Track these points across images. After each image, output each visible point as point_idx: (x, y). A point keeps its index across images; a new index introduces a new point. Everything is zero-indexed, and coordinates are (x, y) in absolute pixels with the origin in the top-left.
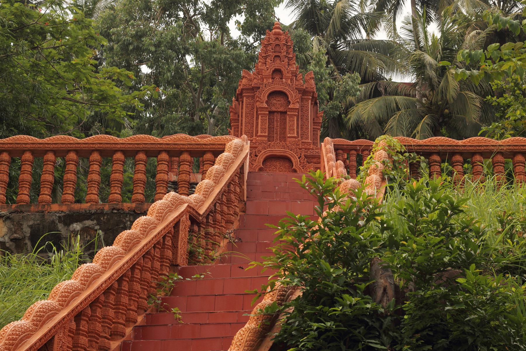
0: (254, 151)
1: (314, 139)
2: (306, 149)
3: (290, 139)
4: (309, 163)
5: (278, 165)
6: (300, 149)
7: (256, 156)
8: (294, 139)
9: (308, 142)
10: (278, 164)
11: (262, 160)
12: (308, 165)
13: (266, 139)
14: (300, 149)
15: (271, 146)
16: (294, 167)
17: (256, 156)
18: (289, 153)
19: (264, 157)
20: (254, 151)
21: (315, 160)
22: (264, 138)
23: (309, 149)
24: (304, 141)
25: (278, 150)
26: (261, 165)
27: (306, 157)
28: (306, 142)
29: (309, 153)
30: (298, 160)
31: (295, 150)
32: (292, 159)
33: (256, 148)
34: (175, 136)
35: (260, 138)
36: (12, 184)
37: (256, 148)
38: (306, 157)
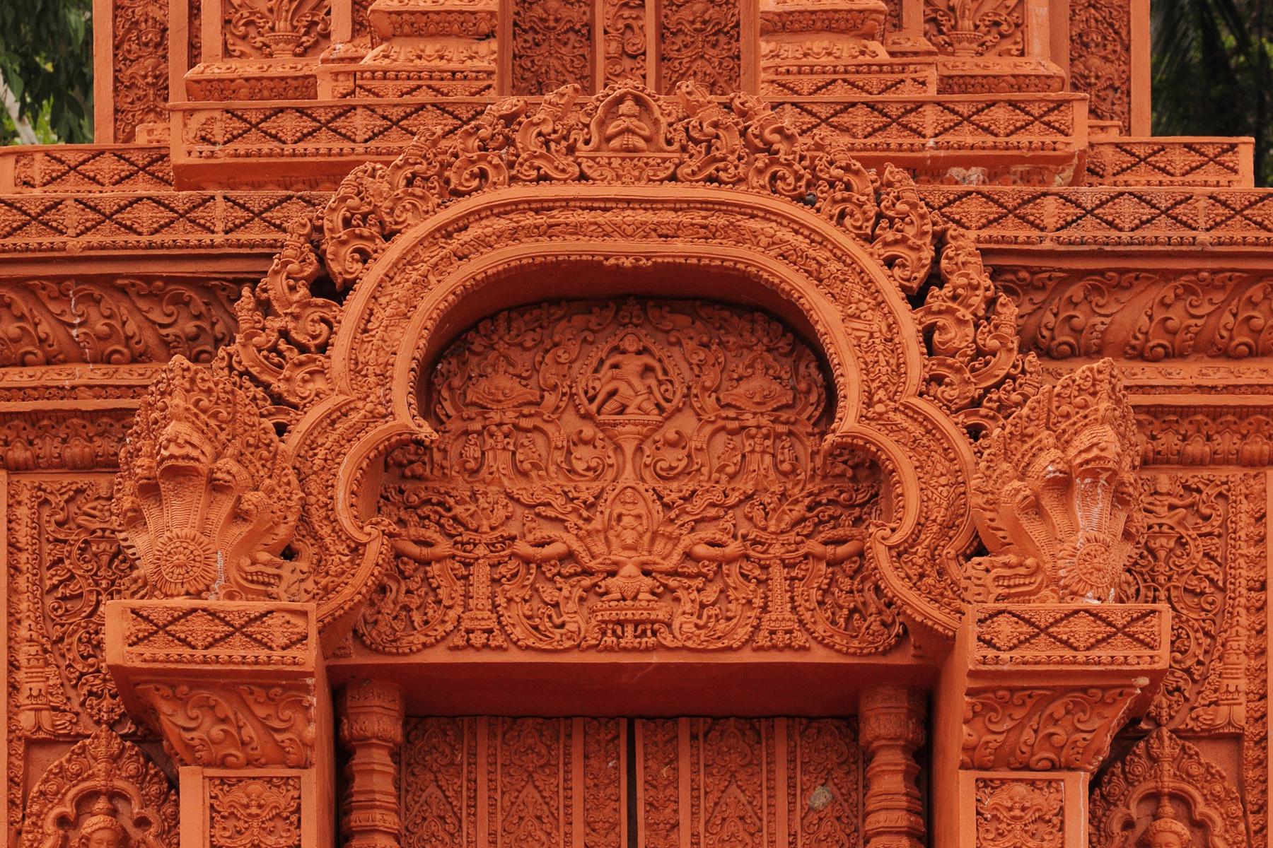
0: (297, 216)
1: (1080, 43)
2: (996, 168)
3: (791, 50)
4: (1046, 353)
5: (633, 388)
6: (917, 169)
7: (329, 288)
8: (846, 48)
9: (1020, 82)
10: (629, 375)
11: (408, 344)
12: (1047, 383)
13: (486, 55)
14: (917, 169)
15: (527, 141)
16: (848, 420)
17: (329, 288)
18: (770, 241)
19: (437, 296)
20: (297, 216)
21: (1130, 314)
22: (456, 53)
23: (1041, 166)
24: (966, 62)
25: (625, 210)
26: (404, 416)
27: (1011, 271)
28: (990, 82)
29: (1049, 223)
30: (909, 322)
31: (864, 185)
32: (825, 313)
33: (333, 172)
34: (12, 403)
35: (402, 54)
36: (1261, 518)
37: (333, 172)
38: (1011, 271)
